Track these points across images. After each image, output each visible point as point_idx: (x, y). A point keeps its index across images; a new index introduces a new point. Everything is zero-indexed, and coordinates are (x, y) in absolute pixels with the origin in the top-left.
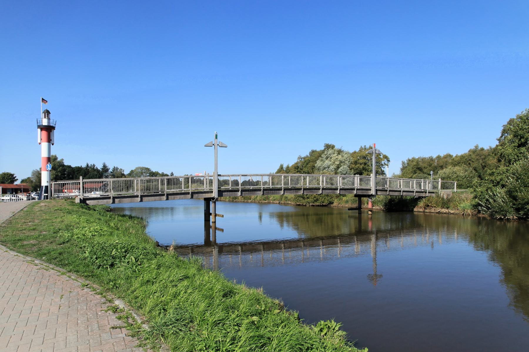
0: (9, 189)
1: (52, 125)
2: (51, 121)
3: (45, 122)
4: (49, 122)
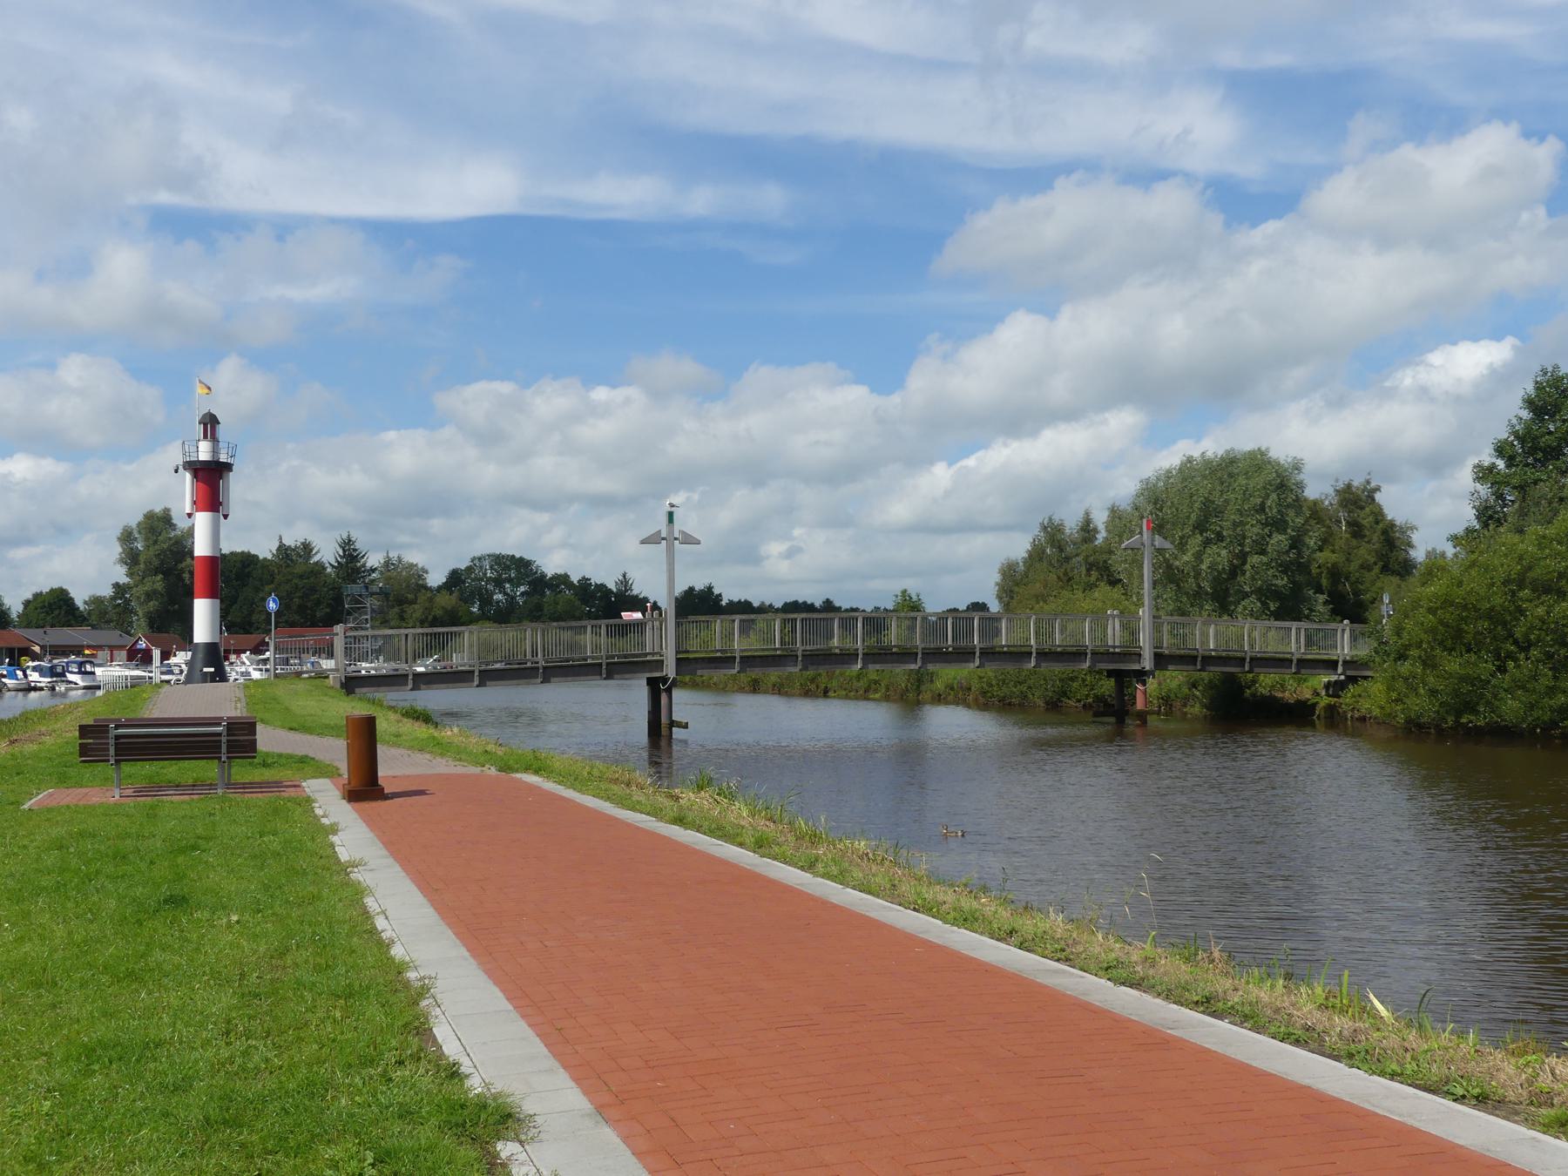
1: (223, 458)
3: (204, 453)
4: (215, 451)
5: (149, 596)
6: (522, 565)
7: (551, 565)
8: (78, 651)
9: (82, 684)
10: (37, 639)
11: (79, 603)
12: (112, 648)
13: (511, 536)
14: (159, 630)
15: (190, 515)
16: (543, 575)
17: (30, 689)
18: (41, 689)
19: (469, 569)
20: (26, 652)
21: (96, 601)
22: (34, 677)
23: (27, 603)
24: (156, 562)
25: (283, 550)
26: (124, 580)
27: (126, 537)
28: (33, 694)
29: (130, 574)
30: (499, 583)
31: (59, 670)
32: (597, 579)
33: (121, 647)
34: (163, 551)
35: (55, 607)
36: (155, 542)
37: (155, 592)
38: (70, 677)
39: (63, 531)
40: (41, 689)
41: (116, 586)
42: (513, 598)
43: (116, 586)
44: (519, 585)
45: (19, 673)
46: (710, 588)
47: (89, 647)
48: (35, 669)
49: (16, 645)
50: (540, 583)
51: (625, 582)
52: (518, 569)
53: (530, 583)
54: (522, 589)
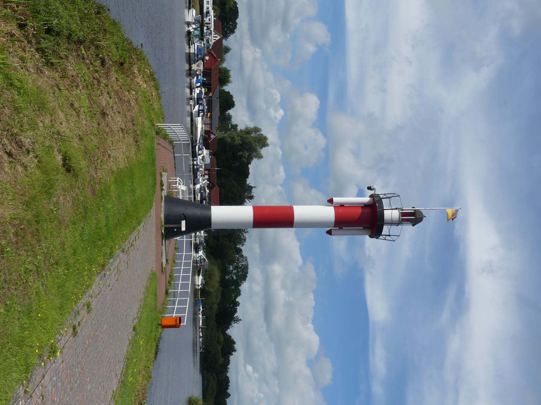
0: (210, 80)
1: (386, 230)
2: (395, 230)
3: (391, 214)
4: (392, 223)
5: (233, 138)
6: (244, 277)
7: (244, 287)
8: (210, 110)
9: (194, 111)
10: (215, 96)
11: (229, 111)
12: (211, 124)
13: (255, 272)
14: (218, 142)
15: (331, 201)
16: (240, 285)
17: (191, 89)
18: (191, 94)
19: (242, 256)
20: (209, 90)
21: (230, 117)
22: (197, 91)
23: (229, 93)
24: (247, 141)
25: (251, 188)
26: (239, 128)
27: (256, 130)
28: (188, 91)
29: (241, 131)
30: (237, 268)
31: (200, 102)
32: (239, 309)
33: (211, 128)
34: (251, 144)
35: (228, 102)
36: (255, 141)
37: (235, 141)
38: (197, 107)
39: (252, 108)
40: (191, 94)
41: (236, 126)
42: (231, 273)
43: (236, 126)
44: (236, 276)
45: (199, 84)
46: (235, 351)
47: (211, 115)
48: (201, 91)
49: (212, 87)
50: (237, 283)
51: (238, 320)
52: (242, 275)
53: (237, 280)
54: (235, 278)
